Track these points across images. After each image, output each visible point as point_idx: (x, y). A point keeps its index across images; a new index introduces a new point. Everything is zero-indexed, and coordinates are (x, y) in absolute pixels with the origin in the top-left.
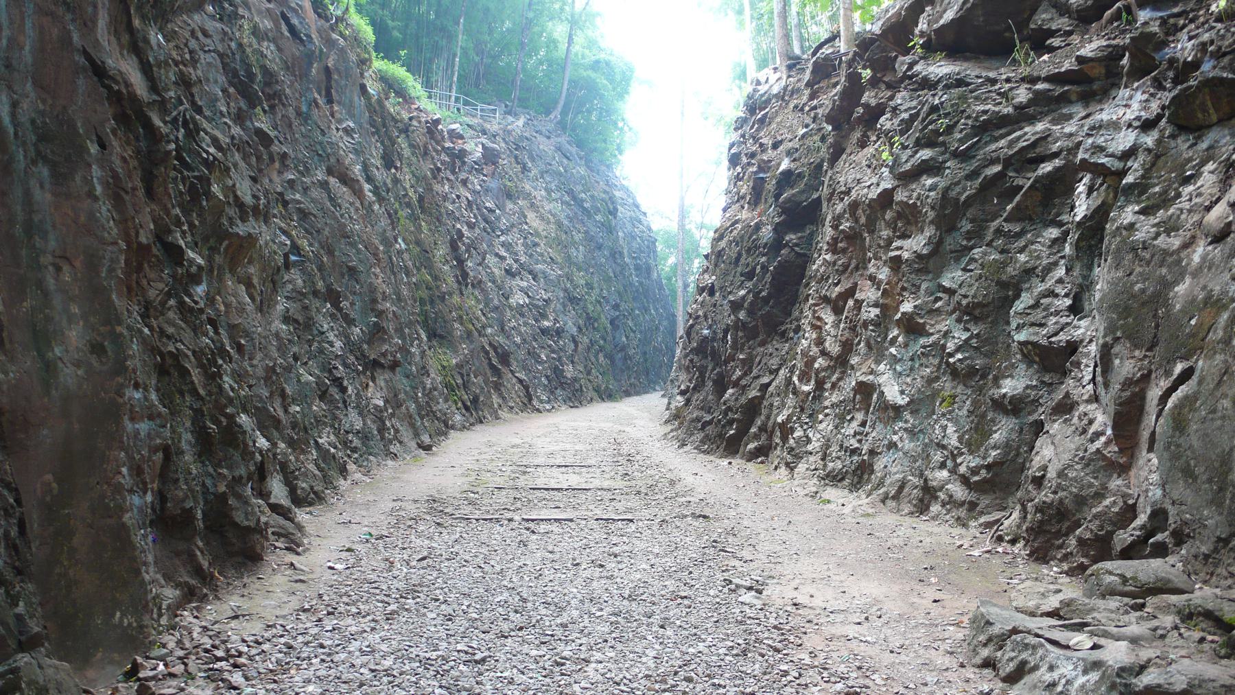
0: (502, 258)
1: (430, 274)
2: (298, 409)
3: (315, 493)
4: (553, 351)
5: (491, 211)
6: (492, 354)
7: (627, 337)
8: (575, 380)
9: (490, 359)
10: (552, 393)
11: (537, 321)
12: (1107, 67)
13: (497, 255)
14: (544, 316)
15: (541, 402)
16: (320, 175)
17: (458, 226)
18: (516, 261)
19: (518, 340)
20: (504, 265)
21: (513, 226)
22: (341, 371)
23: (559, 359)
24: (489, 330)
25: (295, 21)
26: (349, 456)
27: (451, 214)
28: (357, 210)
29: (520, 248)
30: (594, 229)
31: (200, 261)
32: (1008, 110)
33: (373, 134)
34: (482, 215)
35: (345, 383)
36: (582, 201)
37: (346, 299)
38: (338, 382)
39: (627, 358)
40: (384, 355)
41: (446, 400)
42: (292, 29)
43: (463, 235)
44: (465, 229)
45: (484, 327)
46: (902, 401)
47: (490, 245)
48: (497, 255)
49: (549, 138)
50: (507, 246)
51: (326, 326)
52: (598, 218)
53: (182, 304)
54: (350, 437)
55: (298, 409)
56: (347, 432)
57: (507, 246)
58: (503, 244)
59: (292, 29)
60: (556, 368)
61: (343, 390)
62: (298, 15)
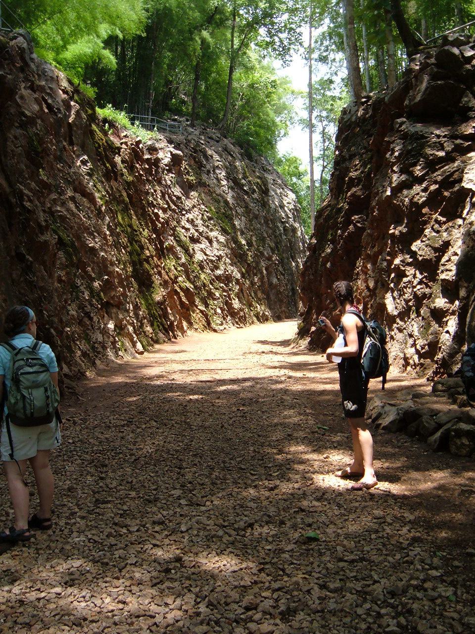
0: (187, 230)
2: (69, 329)
3: (81, 373)
4: (224, 291)
5: (179, 198)
6: (182, 294)
7: (278, 279)
8: (241, 310)
9: (181, 299)
10: (224, 319)
11: (212, 270)
13: (183, 228)
14: (217, 268)
15: (217, 324)
16: (70, 193)
17: (156, 211)
18: (197, 231)
20: (189, 234)
21: (194, 206)
22: (88, 308)
24: (180, 279)
25: (50, 101)
26: (96, 356)
28: (92, 211)
29: (199, 222)
31: (30, 259)
32: (441, 154)
33: (99, 160)
35: (92, 315)
36: (243, 185)
37: (89, 266)
38: (88, 315)
39: (279, 293)
40: (113, 298)
42: (49, 107)
43: (159, 216)
44: (160, 213)
45: (176, 277)
46: (396, 313)
47: (178, 222)
48: (183, 228)
49: (218, 142)
50: (192, 222)
51: (79, 284)
53: (26, 279)
54: (96, 345)
55: (69, 329)
56: (95, 343)
57: (192, 222)
58: (188, 221)
59: (49, 107)
61: (91, 319)
62: (52, 97)
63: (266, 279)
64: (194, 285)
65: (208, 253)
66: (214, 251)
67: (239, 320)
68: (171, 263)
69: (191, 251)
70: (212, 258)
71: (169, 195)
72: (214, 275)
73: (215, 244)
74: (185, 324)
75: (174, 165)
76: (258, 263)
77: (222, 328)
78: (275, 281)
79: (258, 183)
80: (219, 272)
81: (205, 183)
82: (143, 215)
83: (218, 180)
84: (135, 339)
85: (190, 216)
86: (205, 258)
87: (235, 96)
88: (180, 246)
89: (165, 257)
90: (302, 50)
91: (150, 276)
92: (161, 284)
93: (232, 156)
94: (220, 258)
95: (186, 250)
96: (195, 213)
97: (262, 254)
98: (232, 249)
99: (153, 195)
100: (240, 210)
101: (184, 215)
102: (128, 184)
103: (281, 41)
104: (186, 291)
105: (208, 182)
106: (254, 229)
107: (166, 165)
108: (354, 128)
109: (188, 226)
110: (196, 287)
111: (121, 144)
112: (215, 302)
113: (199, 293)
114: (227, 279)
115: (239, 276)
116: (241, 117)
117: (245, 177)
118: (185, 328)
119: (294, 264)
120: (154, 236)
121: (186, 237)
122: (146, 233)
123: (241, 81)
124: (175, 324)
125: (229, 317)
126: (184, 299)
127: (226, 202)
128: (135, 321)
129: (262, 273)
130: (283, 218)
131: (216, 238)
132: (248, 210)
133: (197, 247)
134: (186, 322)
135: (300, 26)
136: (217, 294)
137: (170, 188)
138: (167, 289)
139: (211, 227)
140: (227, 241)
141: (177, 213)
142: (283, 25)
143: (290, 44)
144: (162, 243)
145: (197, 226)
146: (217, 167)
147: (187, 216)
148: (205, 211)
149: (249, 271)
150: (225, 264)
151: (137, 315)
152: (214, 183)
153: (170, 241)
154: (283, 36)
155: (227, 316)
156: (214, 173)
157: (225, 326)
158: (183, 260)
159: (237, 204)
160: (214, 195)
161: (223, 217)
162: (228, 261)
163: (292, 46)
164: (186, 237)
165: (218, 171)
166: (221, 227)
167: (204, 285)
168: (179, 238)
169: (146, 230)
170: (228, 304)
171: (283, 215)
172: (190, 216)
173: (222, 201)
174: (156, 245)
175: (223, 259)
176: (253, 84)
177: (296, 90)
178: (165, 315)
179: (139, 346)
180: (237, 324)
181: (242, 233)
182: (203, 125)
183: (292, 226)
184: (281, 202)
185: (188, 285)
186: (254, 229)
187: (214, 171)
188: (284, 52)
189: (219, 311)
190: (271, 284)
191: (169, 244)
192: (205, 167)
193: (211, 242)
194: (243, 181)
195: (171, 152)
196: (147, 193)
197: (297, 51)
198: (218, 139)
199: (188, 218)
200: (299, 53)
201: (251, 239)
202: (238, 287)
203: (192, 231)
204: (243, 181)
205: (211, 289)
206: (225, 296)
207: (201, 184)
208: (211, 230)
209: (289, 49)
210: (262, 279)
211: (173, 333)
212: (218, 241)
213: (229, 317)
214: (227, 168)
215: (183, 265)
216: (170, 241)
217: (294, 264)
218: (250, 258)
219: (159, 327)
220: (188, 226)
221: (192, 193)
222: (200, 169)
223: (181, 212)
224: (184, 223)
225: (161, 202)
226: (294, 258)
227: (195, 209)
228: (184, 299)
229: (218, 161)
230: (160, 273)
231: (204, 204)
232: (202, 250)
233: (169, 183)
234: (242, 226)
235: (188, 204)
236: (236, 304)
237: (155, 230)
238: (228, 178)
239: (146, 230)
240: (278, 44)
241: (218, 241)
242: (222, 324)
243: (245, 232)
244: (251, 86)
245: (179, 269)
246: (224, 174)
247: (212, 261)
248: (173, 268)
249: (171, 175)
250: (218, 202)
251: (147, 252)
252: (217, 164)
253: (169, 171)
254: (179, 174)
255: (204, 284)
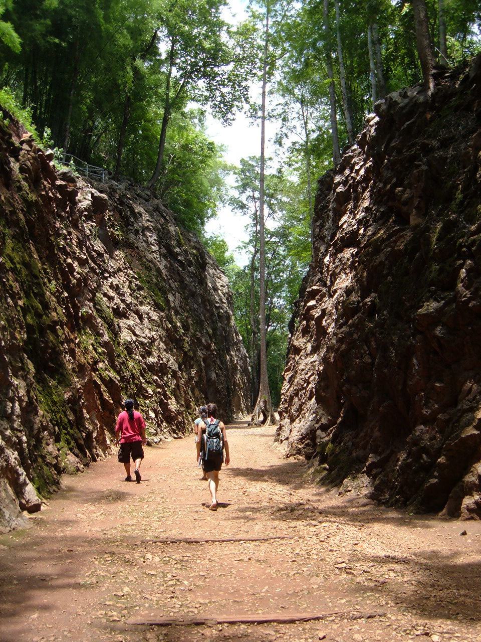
0: (111, 299)
1: (41, 303)
4: (158, 386)
5: (100, 255)
7: (217, 374)
8: (180, 413)
10: (159, 426)
11: (144, 357)
12: (33, 437)
13: (105, 295)
14: (149, 354)
17: (69, 261)
18: (123, 301)
19: (127, 374)
20: (112, 305)
21: (119, 270)
23: (165, 394)
24: (101, 365)
27: (63, 250)
29: (126, 290)
30: (188, 279)
34: (92, 257)
36: (178, 254)
41: (57, 440)
43: (74, 270)
44: (76, 264)
45: (96, 362)
47: (99, 286)
48: (105, 295)
49: (147, 200)
50: (116, 288)
52: (191, 269)
57: (116, 288)
58: (111, 287)
60: (161, 401)
63: (204, 374)
64: (119, 375)
65: (138, 333)
66: (146, 332)
67: (177, 427)
68: (87, 340)
69: (116, 327)
70: (144, 340)
71: (87, 248)
72: (145, 363)
73: (146, 321)
74: (107, 435)
75: (95, 212)
76: (195, 352)
77: (156, 439)
78: (213, 376)
79: (194, 254)
80: (152, 360)
81: (133, 244)
82: (50, 253)
83: (149, 244)
84: (22, 478)
85: (114, 281)
86: (134, 338)
87: (165, 158)
88: (101, 317)
89: (79, 332)
90: (247, 107)
91: (59, 353)
92: (73, 369)
93: (164, 218)
94: (153, 340)
95: (110, 326)
96: (119, 281)
97: (199, 340)
98: (167, 330)
99: (65, 239)
100: (174, 285)
101: (106, 278)
102: (28, 204)
103: (222, 95)
104: (109, 383)
105: (137, 244)
106: (190, 309)
107: (86, 210)
108: (424, 113)
109: (111, 293)
110: (123, 379)
111: (22, 143)
112: (147, 402)
113: (126, 388)
114: (161, 369)
115: (175, 367)
116: (173, 183)
117: (180, 246)
118: (108, 442)
119: (228, 357)
120: (66, 294)
121: (109, 307)
122: (53, 285)
123: (174, 144)
124: (95, 435)
125: (164, 423)
126: (106, 396)
127: (158, 271)
128: (24, 439)
129: (200, 365)
130: (217, 303)
131: (148, 314)
132: (183, 286)
133: (123, 323)
134: (109, 431)
135: (246, 79)
136: (150, 391)
137: (89, 240)
138: (84, 378)
139: (141, 299)
140: (161, 318)
141: (97, 274)
142: (226, 76)
143: (233, 100)
144: (77, 309)
145: (124, 295)
146: (148, 228)
147: (110, 280)
148: (133, 277)
149: (186, 362)
150: (159, 349)
151: (27, 423)
152: (143, 247)
153: (87, 309)
154: (225, 90)
155: (162, 422)
156: (144, 235)
157: (160, 436)
158: (106, 338)
159: (171, 276)
160: (145, 260)
161: (156, 289)
162: (162, 345)
163: (236, 103)
164: (109, 307)
165: (148, 234)
166: (153, 300)
167: (133, 377)
168: (100, 306)
169: (53, 282)
170: (164, 405)
171: (217, 299)
172: (114, 281)
173: (154, 269)
174: (67, 309)
175: (156, 343)
176: (187, 145)
177: (229, 164)
178: (79, 422)
179: (30, 491)
180: (174, 432)
181: (177, 313)
182: (130, 180)
183: (226, 312)
184: (214, 283)
185: (112, 374)
186: (190, 309)
187: (143, 232)
188: (225, 109)
189: (152, 414)
190: (209, 380)
191: (87, 312)
192: (132, 226)
193: (141, 318)
194: (177, 250)
195: (92, 194)
196: (57, 234)
197: (240, 109)
198: (147, 197)
199: (112, 283)
200: (243, 111)
201: (186, 321)
202: (174, 382)
203: (117, 300)
204: (177, 250)
205: (141, 383)
206: (159, 393)
207: (127, 245)
208: (141, 303)
209: (232, 106)
210: (199, 373)
211: (91, 451)
212: (149, 318)
213: (164, 423)
214: (159, 230)
215: (106, 345)
216: (87, 309)
217: (228, 357)
218: (186, 345)
219: (69, 444)
220: (111, 293)
221: (117, 252)
222: (126, 227)
223: (102, 274)
224: (106, 289)
225: (77, 250)
226: (228, 351)
227: (121, 273)
228: (106, 396)
229: (148, 220)
230: (72, 353)
231: (132, 270)
232: (130, 328)
233: (88, 232)
234: (177, 304)
235: (112, 265)
236: (173, 405)
237: (67, 286)
238: (159, 242)
239: (53, 282)
240: (219, 99)
241: (149, 318)
242: (155, 435)
243: (180, 312)
244: (186, 148)
245: (100, 350)
246: (155, 237)
247: (142, 344)
248: (91, 348)
249: (91, 223)
250: (149, 269)
251: (54, 314)
252: (146, 224)
253: (89, 218)
254: (102, 224)
255: (133, 374)
